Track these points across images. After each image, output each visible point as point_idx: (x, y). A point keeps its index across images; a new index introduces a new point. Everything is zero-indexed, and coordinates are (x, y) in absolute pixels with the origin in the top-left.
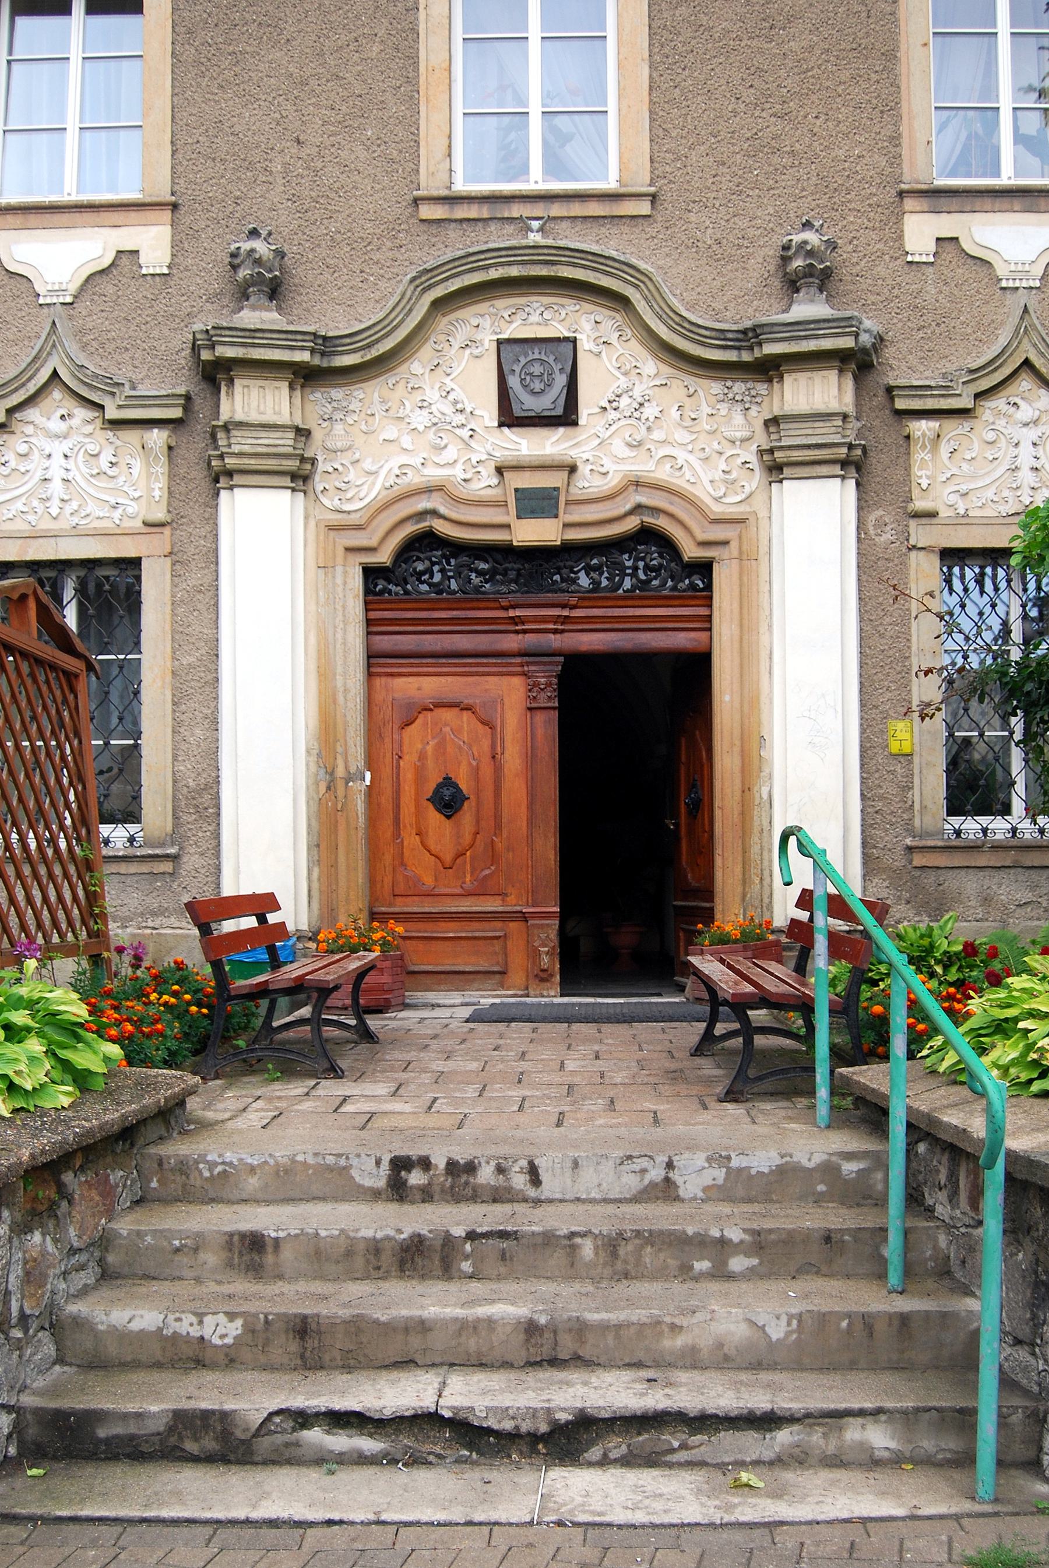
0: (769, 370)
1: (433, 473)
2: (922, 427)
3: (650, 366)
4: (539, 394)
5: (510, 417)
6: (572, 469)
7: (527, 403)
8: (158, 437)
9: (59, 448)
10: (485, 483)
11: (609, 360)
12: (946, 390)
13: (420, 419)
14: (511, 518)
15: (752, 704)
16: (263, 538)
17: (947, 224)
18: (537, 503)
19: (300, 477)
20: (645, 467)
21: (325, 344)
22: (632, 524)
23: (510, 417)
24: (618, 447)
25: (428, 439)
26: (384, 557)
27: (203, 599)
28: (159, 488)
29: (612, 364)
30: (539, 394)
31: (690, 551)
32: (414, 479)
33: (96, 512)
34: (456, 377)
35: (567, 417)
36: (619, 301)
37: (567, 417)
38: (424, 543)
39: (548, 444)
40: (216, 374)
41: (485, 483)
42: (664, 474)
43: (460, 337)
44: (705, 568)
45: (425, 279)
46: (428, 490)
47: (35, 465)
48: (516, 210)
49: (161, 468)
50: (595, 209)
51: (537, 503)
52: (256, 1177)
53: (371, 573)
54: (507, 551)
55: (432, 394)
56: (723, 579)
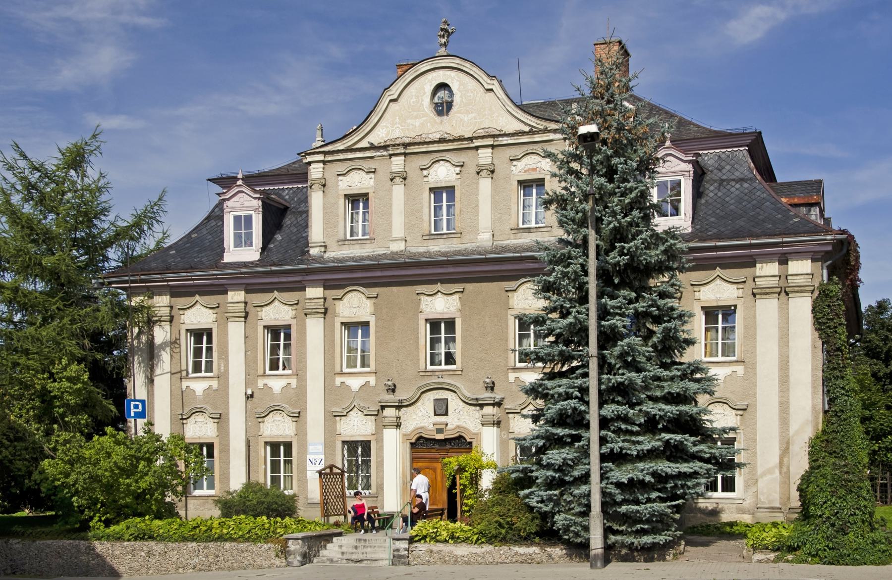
0: (482, 406)
1: (422, 425)
2: (511, 416)
3: (462, 404)
4: (441, 409)
5: (436, 414)
6: (447, 425)
7: (438, 412)
8: (373, 418)
9: (356, 419)
10: (431, 427)
11: (454, 403)
12: (515, 409)
13: (420, 414)
14: (435, 433)
15: (814, 375)
16: (391, 437)
17: (517, 375)
18: (440, 431)
19: (398, 426)
20: (461, 424)
21: (401, 401)
22: (457, 435)
23: (436, 414)
24: (456, 420)
25: (421, 418)
26: (413, 441)
27: (381, 448)
28: (374, 427)
29: (454, 403)
30: (441, 409)
31: (468, 440)
32: (419, 426)
33: (363, 432)
34: (427, 403)
35: (446, 414)
36: (455, 392)
37: (446, 414)
38: (420, 438)
39: (443, 419)
40: (383, 407)
41: (431, 427)
42: (464, 425)
43: (427, 398)
44: (471, 443)
45: (419, 388)
46: (421, 428)
47: (352, 422)
48: (437, 373)
49: (374, 424)
50: (451, 373)
51: (440, 431)
52: (143, 434)
53: (412, 444)
54: (434, 440)
55: (422, 409)
56: (474, 445)
